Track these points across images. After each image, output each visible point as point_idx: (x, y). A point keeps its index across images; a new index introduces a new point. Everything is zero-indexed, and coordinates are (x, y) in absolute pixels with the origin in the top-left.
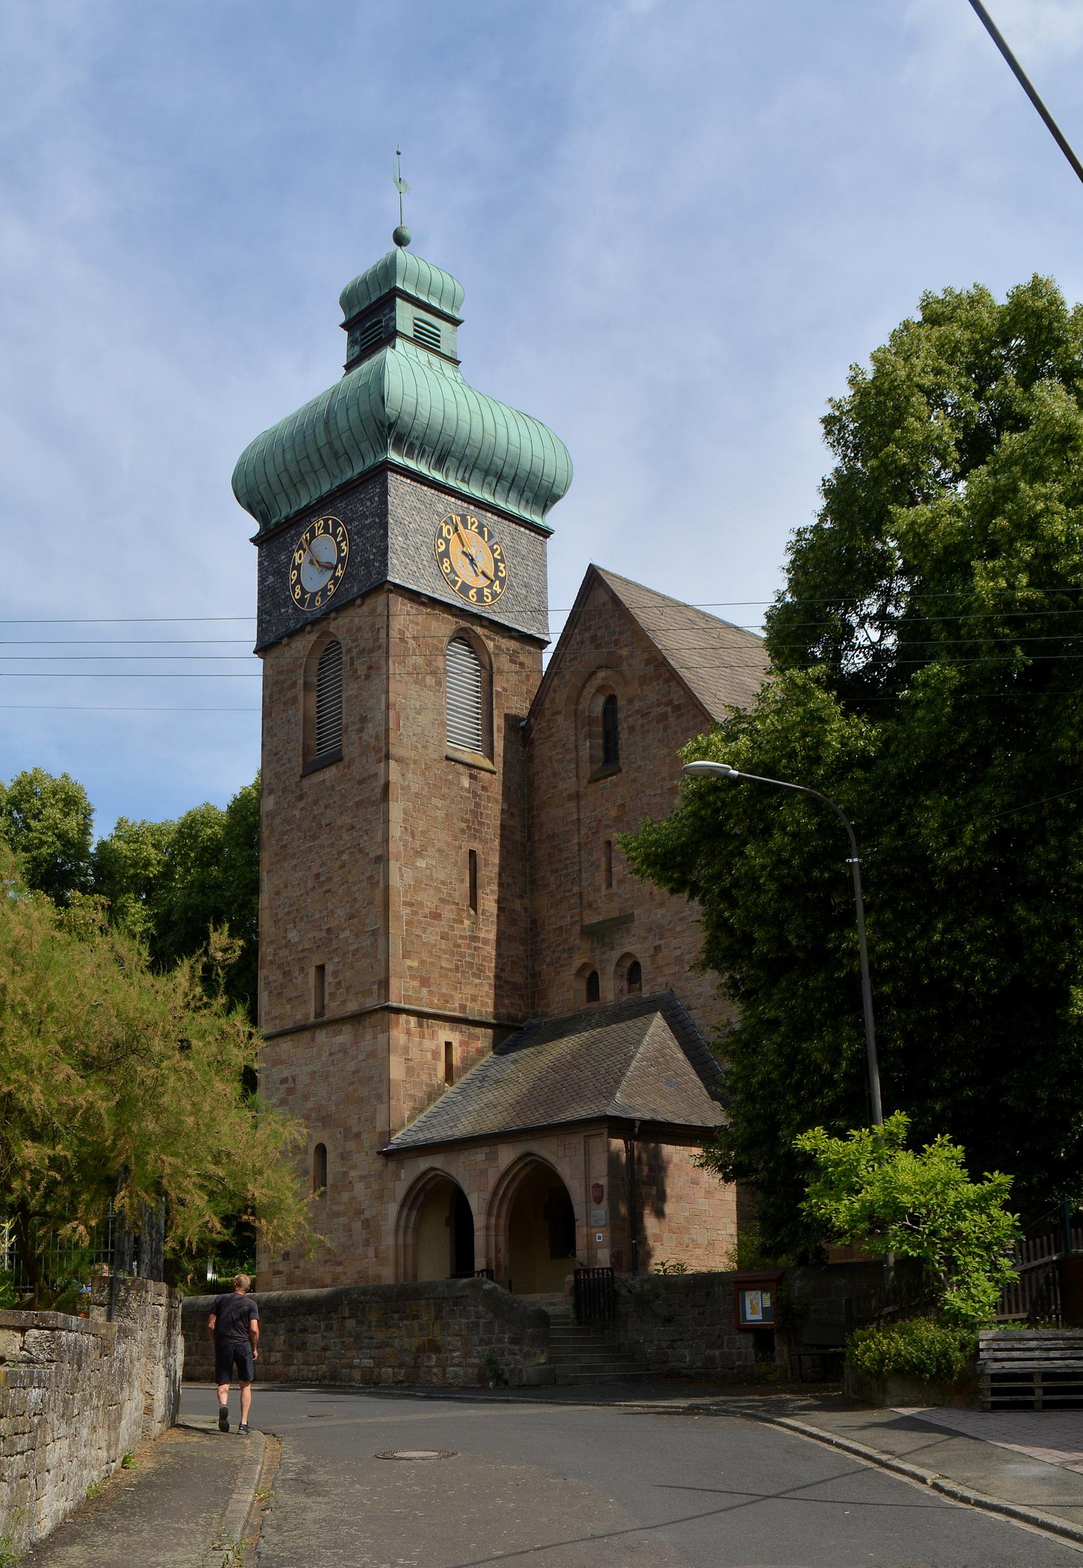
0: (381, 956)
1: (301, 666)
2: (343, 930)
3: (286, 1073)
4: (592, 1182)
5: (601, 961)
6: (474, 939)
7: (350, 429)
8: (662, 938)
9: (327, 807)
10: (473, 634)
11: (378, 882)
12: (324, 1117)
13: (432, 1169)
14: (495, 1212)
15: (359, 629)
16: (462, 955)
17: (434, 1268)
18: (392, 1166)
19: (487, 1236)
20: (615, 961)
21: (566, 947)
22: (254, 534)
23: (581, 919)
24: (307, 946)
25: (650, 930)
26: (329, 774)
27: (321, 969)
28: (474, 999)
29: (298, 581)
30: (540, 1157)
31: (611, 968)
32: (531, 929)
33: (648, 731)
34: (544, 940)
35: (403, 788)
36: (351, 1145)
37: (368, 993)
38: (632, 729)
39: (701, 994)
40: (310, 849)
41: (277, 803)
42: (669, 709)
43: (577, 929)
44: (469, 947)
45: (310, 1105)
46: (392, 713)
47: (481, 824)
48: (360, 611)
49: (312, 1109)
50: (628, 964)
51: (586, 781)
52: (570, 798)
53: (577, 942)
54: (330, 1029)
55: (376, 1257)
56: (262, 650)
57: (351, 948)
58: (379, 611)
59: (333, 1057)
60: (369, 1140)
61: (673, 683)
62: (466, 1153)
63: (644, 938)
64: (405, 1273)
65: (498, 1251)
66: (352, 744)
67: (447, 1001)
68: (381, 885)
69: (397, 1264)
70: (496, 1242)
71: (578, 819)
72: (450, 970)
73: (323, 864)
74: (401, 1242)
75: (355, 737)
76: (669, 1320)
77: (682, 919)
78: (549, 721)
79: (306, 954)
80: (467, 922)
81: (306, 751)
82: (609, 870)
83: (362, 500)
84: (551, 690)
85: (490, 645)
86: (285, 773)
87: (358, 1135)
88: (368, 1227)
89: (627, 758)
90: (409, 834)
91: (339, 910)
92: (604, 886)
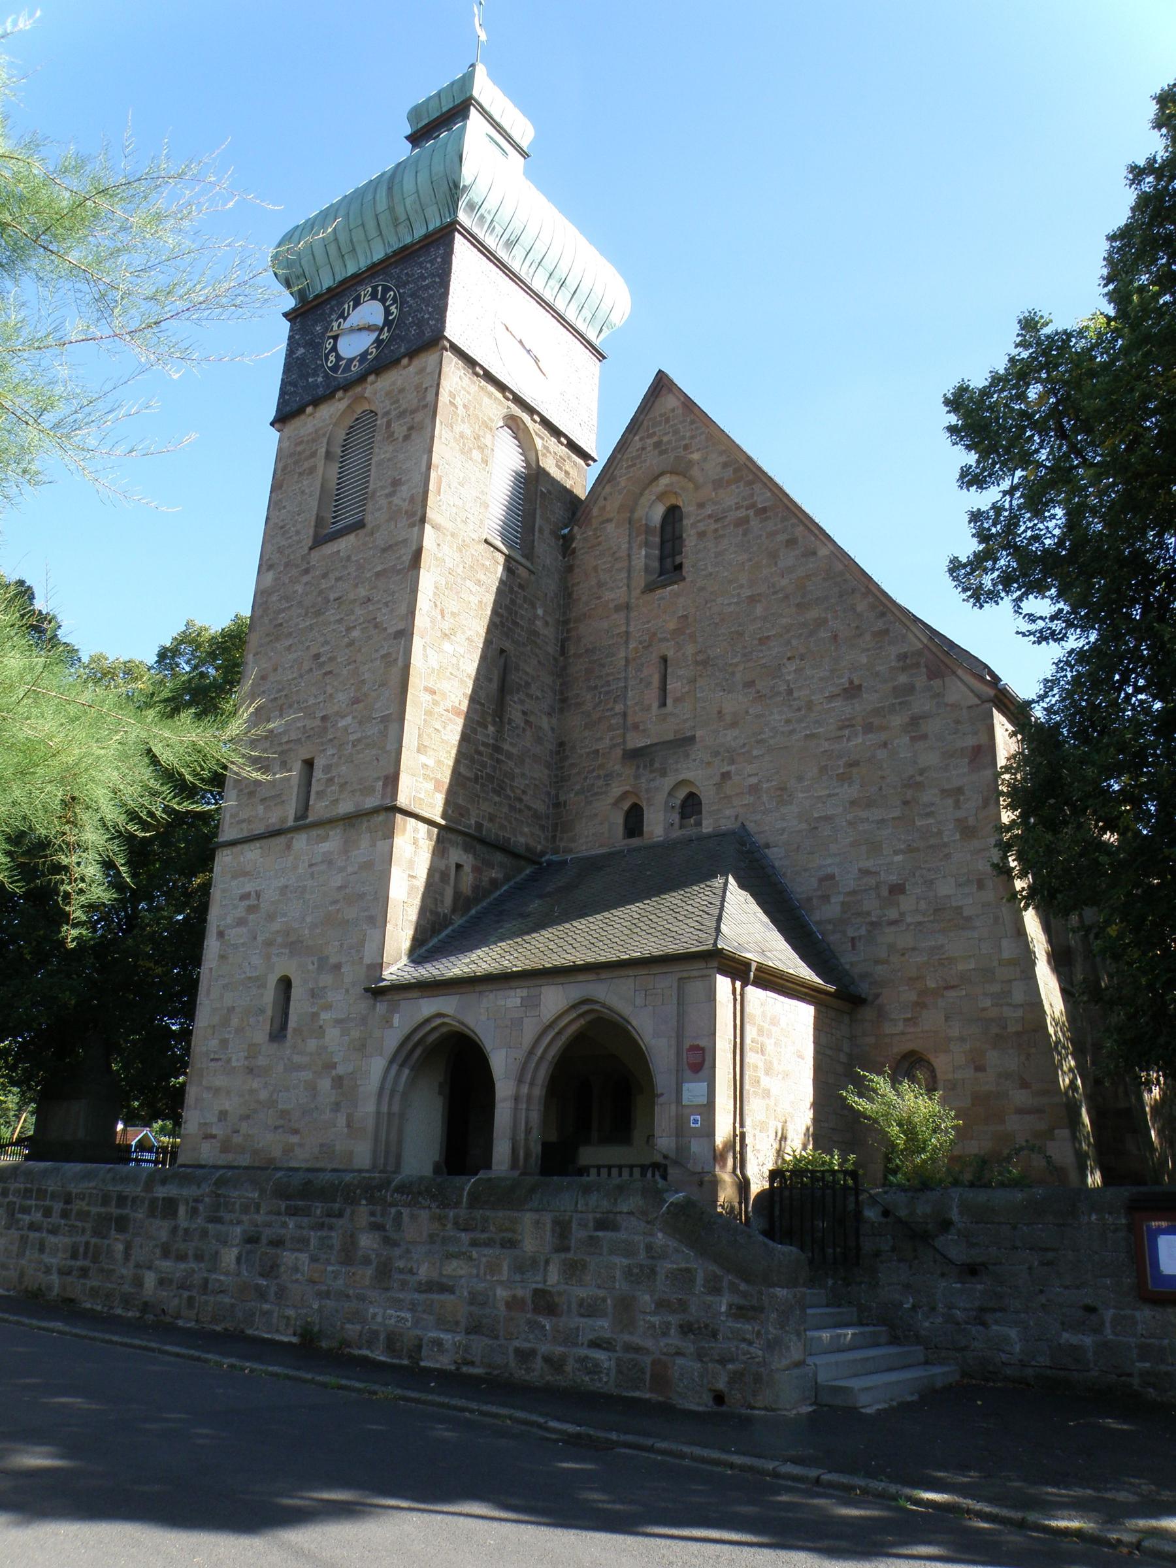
0: (390, 746)
1: (324, 435)
2: (343, 717)
3: (249, 887)
4: (687, 1044)
5: (648, 791)
6: (497, 749)
7: (417, 191)
8: (732, 762)
9: (338, 579)
10: (522, 426)
11: (396, 660)
12: (292, 943)
13: (440, 1015)
14: (528, 1077)
15: (402, 391)
16: (484, 765)
17: (421, 1150)
18: (381, 1007)
19: (516, 1110)
20: (667, 789)
21: (602, 773)
22: (287, 309)
23: (624, 742)
24: (293, 737)
25: (716, 754)
26: (344, 544)
27: (309, 764)
28: (492, 818)
29: (334, 348)
30: (604, 1005)
31: (661, 797)
32: (558, 753)
33: (723, 536)
34: (573, 765)
35: (436, 559)
36: (327, 979)
37: (368, 791)
38: (702, 535)
39: (784, 830)
40: (311, 628)
41: (276, 579)
42: (751, 512)
43: (619, 752)
44: (491, 757)
45: (276, 926)
46: (433, 474)
47: (515, 623)
48: (404, 372)
49: (278, 932)
50: (682, 794)
51: (638, 591)
52: (617, 609)
53: (617, 767)
54: (314, 833)
55: (348, 1126)
56: (282, 419)
57: (352, 738)
58: (428, 370)
59: (314, 869)
60: (352, 974)
61: (757, 487)
62: (491, 996)
63: (709, 763)
64: (387, 1153)
65: (528, 1131)
66: (379, 509)
67: (462, 815)
68: (400, 663)
69: (376, 1139)
70: (527, 1117)
71: (627, 632)
72: (468, 779)
73: (327, 643)
74: (385, 1109)
75: (383, 502)
76: (972, 1270)
77: (759, 742)
78: (596, 529)
79: (291, 745)
80: (491, 729)
81: (319, 522)
82: (663, 689)
83: (422, 263)
84: (601, 498)
85: (539, 443)
86: (290, 546)
87: (338, 967)
88: (341, 1086)
89: (693, 566)
90: (438, 611)
91: (340, 694)
92: (655, 705)
